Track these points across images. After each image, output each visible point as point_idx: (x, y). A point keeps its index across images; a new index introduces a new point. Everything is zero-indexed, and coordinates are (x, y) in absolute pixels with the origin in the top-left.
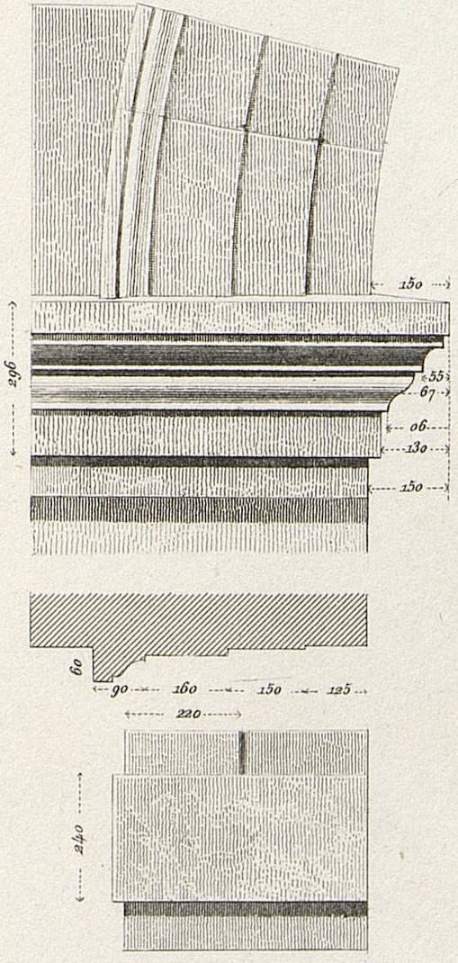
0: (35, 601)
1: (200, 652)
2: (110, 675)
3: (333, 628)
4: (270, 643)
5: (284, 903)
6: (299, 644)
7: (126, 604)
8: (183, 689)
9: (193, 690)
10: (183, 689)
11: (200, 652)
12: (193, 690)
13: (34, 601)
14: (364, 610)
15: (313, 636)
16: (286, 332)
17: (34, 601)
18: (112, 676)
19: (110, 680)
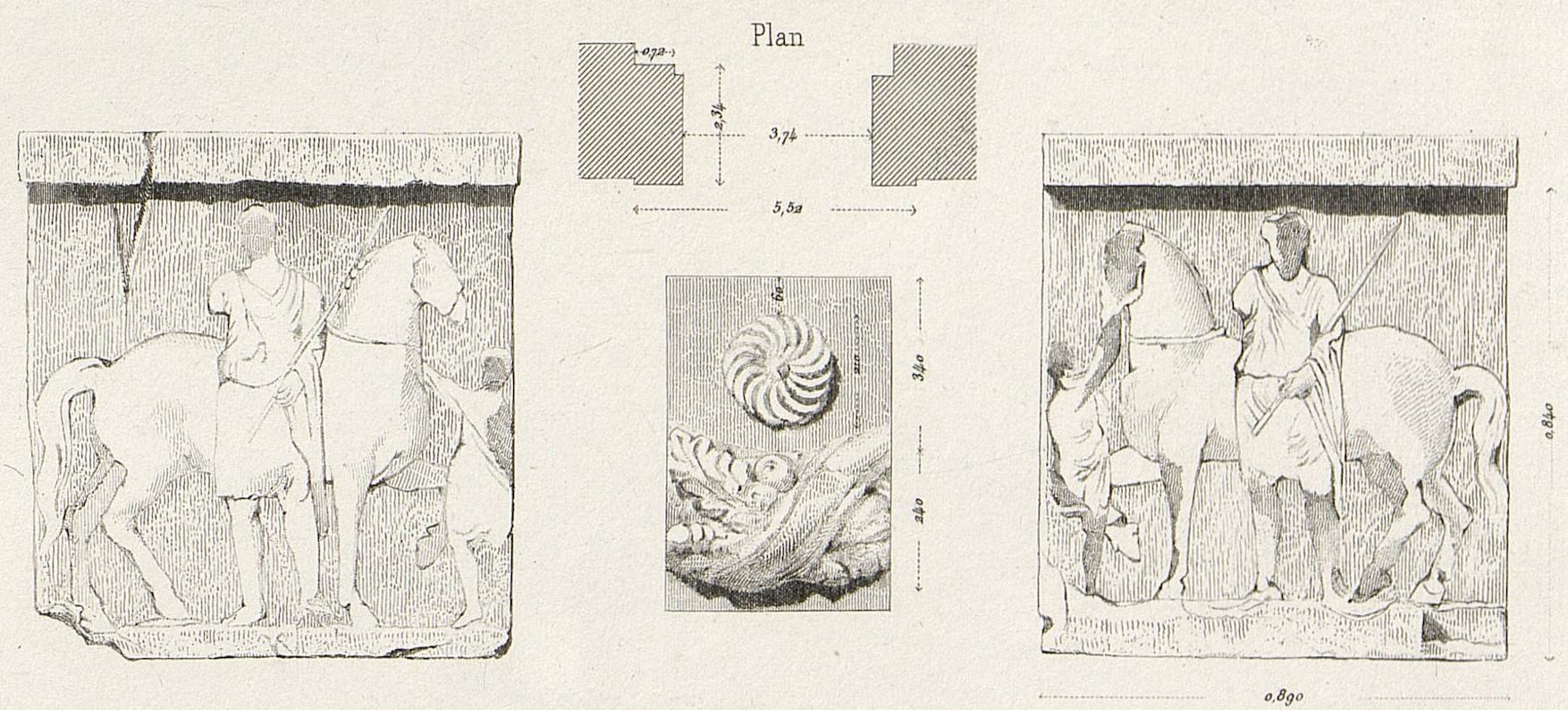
0: (876, 170)
1: (624, 175)
2: (914, 178)
3: (655, 75)
4: (627, 172)
5: (1152, 186)
6: (890, 81)
7: (665, 157)
8: (292, 634)
9: (1299, 697)
10: (292, 634)
11: (624, 175)
12: (1299, 697)
13: (966, 172)
14: (875, 96)
15: (655, 173)
16: (1132, 184)
17: (966, 172)
18: (916, 179)
19: (914, 183)
